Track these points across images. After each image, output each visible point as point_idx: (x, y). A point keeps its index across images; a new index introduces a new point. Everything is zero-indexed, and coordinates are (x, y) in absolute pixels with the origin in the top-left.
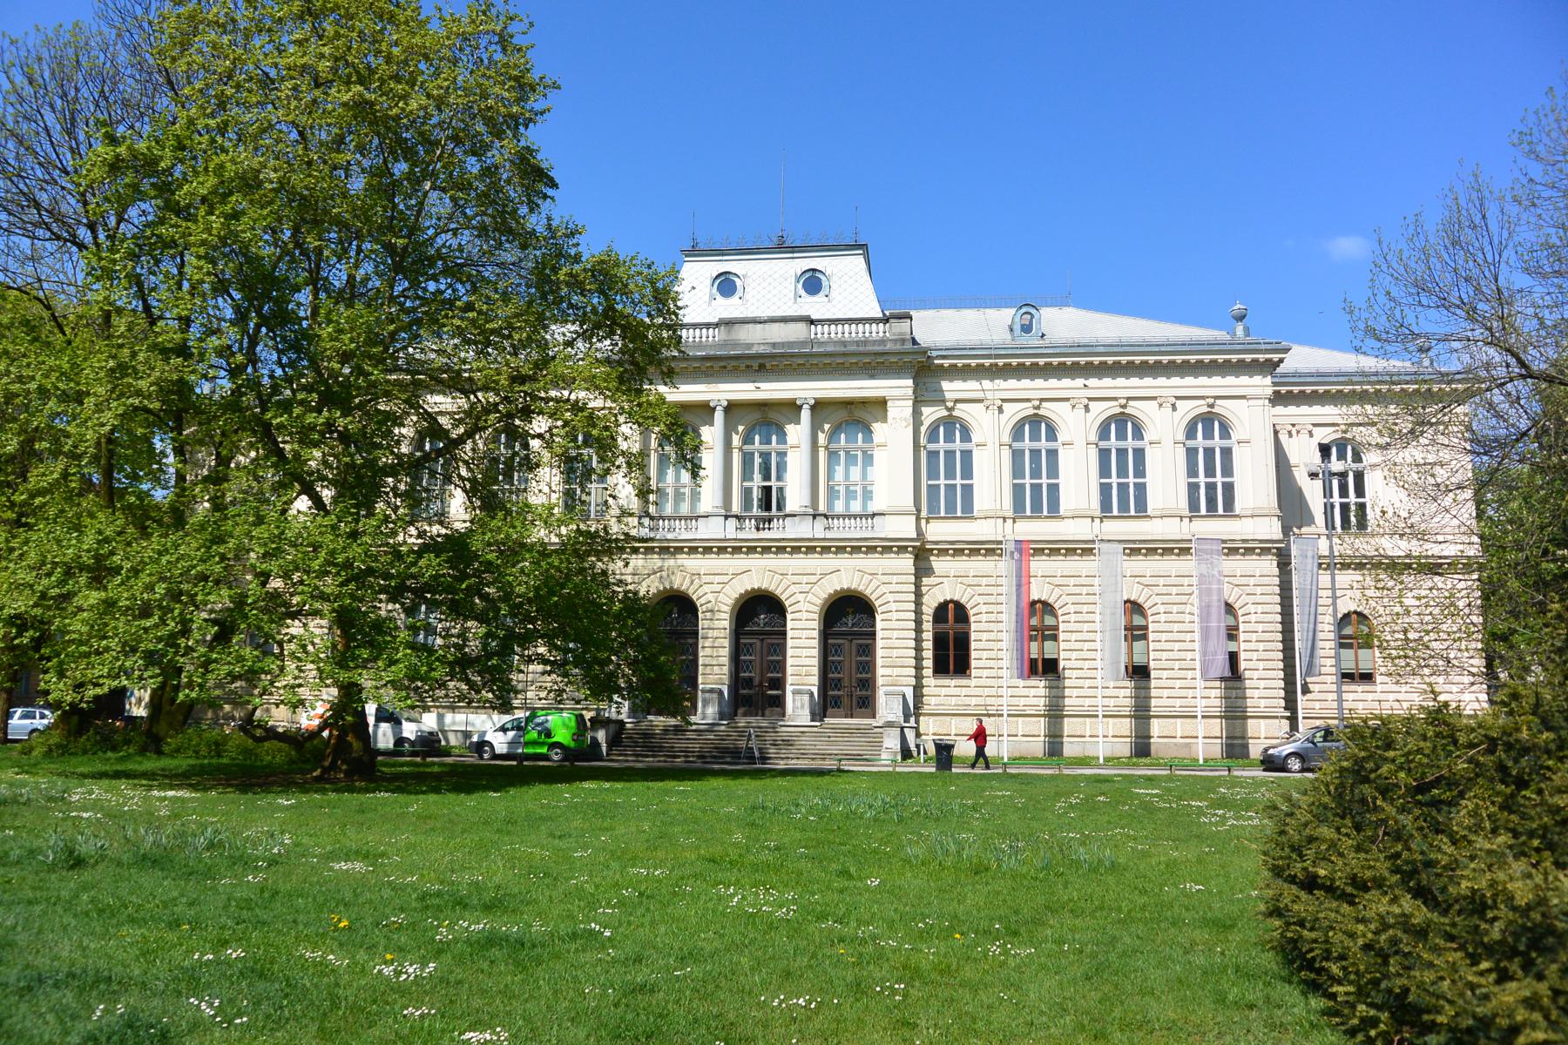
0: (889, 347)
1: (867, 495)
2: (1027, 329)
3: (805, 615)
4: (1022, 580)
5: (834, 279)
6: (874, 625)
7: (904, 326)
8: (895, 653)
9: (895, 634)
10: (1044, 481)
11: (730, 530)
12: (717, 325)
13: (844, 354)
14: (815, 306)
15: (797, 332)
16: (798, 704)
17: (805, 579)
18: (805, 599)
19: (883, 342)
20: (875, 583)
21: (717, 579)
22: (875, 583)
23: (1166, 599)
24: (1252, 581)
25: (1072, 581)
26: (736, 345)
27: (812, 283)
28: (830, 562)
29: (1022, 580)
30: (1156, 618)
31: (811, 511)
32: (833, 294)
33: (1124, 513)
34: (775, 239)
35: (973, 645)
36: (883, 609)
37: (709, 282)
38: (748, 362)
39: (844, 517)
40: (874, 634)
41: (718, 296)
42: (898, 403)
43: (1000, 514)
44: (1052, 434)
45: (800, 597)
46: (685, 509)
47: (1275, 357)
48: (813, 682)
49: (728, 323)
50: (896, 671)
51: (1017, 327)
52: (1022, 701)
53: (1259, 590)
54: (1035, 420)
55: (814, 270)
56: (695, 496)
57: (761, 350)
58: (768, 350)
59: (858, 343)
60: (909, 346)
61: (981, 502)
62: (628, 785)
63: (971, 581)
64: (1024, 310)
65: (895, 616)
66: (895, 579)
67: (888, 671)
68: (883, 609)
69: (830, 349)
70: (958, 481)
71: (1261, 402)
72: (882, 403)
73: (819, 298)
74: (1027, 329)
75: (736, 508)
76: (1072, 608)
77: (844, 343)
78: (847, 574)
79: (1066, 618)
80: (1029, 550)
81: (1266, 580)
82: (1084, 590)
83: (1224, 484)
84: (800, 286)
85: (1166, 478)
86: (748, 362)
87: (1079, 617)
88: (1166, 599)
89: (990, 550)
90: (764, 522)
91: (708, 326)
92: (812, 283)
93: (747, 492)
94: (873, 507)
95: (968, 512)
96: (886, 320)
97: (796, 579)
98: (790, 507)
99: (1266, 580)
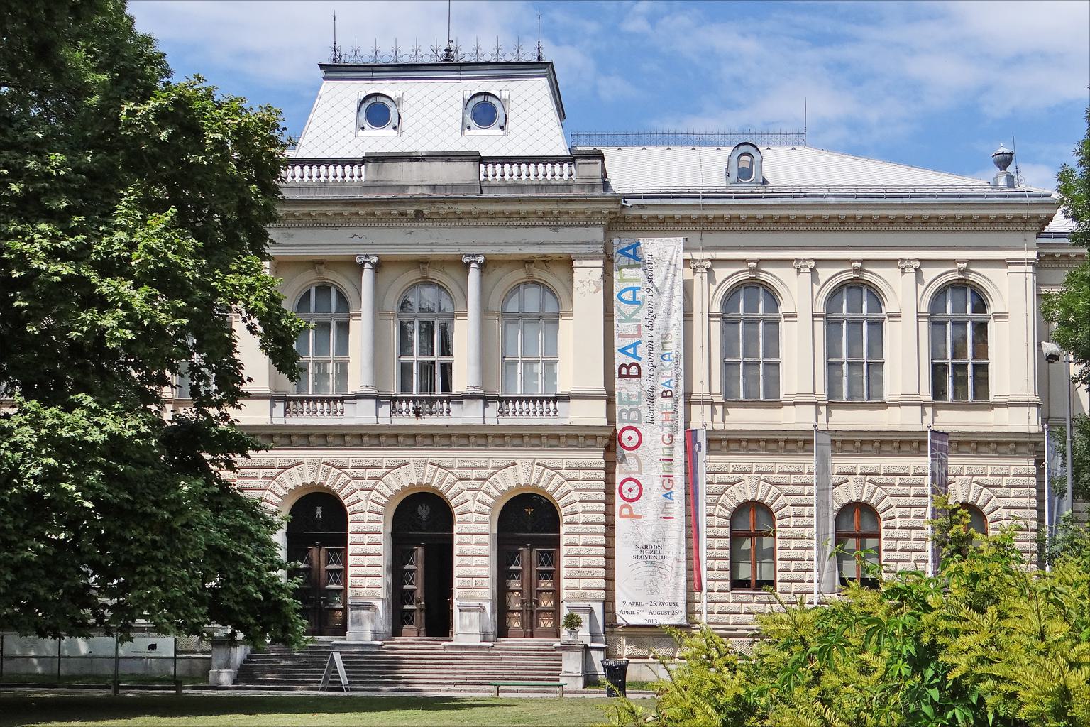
0: (576, 192)
1: (550, 375)
2: (745, 174)
3: (474, 517)
4: (941, 483)
5: (511, 105)
6: (558, 531)
7: (593, 169)
8: (582, 561)
9: (582, 539)
10: (969, 360)
11: (385, 416)
12: (361, 162)
13: (520, 201)
14: (486, 141)
15: (462, 173)
16: (466, 621)
17: (474, 474)
18: (475, 495)
19: (567, 186)
20: (558, 479)
21: (368, 473)
22: (558, 479)
23: (902, 500)
24: (1005, 481)
25: (792, 479)
26: (386, 187)
27: (484, 111)
28: (384, 457)
29: (941, 483)
30: (891, 522)
31: (373, 392)
32: (510, 125)
33: (960, 403)
34: (442, 52)
35: (457, 550)
36: (354, 507)
37: (355, 107)
38: (402, 208)
39: (315, 400)
40: (558, 538)
41: (366, 124)
42: (585, 263)
43: (707, 397)
44: (981, 304)
45: (469, 495)
46: (331, 388)
47: (1043, 213)
48: (486, 594)
49: (378, 159)
50: (583, 583)
51: (734, 172)
52: (732, 618)
53: (1012, 492)
54: (856, 285)
55: (486, 94)
56: (343, 375)
57: (418, 193)
58: (427, 193)
59: (538, 187)
60: (599, 192)
61: (998, 387)
62: (170, 718)
63: (775, 478)
64: (743, 149)
65: (582, 518)
66: (581, 474)
67: (574, 583)
68: (354, 507)
69: (504, 194)
70: (437, 358)
71: (1023, 269)
72: (568, 262)
73: (494, 131)
74: (745, 174)
75: (394, 388)
76: (791, 511)
77: (522, 187)
78: (522, 470)
79: (784, 521)
80: (847, 443)
81: (1022, 480)
82: (913, 491)
83: (421, 364)
84: (362, 117)
85: (800, 354)
86: (402, 208)
87: (800, 521)
88: (902, 500)
89: (796, 442)
90: (425, 403)
91: (352, 162)
92: (484, 111)
93: (406, 369)
94: (563, 387)
95: (981, 399)
96: (571, 160)
97: (359, 472)
98: (458, 386)
99: (1022, 480)
